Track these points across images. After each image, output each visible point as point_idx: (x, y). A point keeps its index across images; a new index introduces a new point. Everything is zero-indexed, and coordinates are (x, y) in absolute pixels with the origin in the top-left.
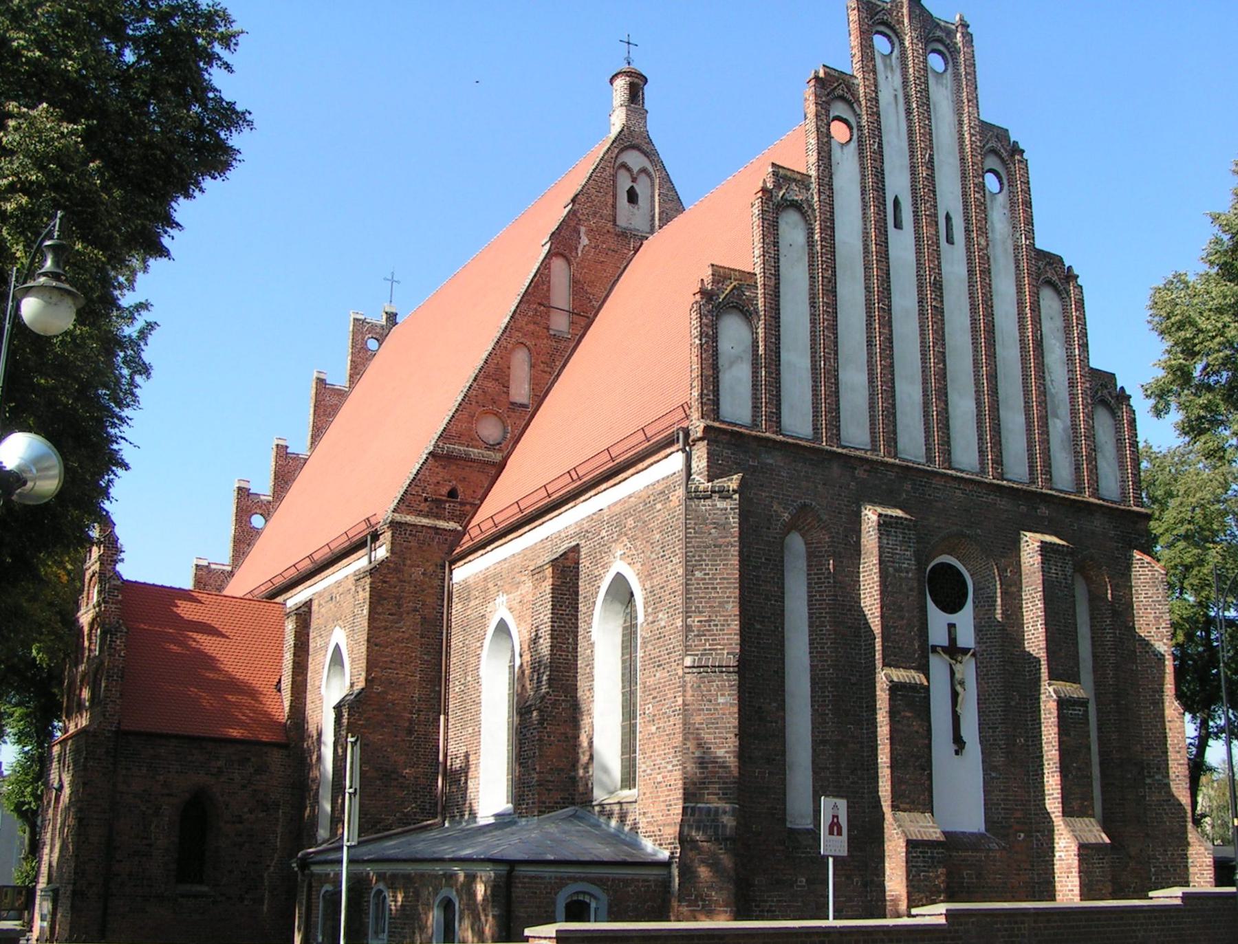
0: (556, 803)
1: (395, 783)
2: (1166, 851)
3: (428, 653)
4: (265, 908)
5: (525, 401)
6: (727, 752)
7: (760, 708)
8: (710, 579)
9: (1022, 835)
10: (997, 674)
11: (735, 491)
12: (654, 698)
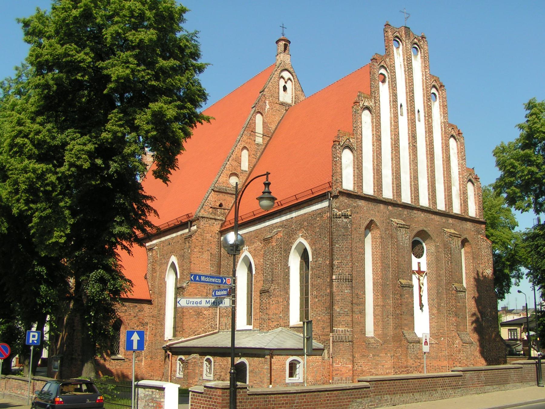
1: (201, 317)
2: (490, 344)
3: (213, 267)
4: (143, 364)
5: (247, 169)
7: (357, 293)
9: (443, 338)
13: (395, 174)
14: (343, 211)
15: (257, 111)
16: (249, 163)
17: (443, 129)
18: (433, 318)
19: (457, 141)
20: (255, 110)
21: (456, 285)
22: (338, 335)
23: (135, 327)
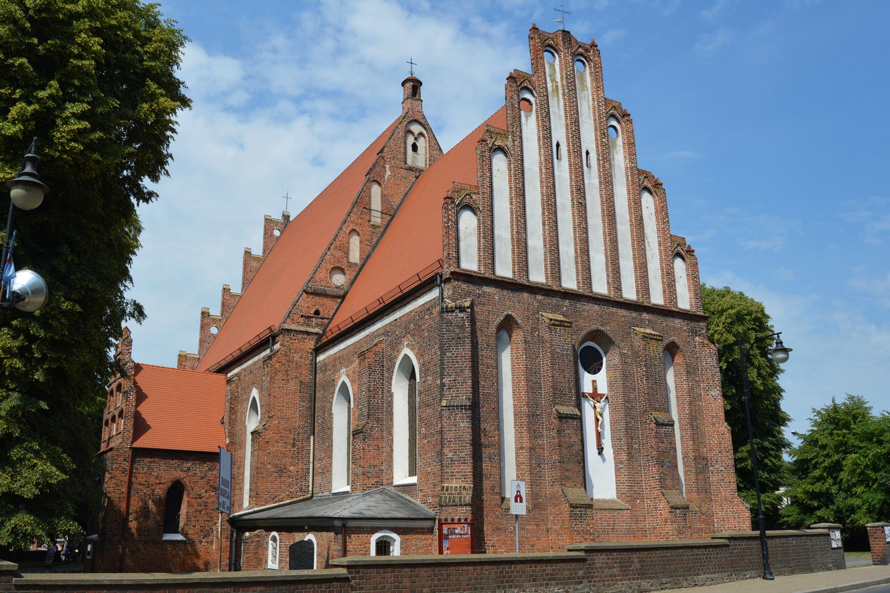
0: (372, 485)
3: (304, 402)
5: (358, 262)
6: (466, 455)
8: (455, 357)
9: (638, 501)
10: (621, 408)
11: (468, 308)
12: (425, 424)
13: (548, 246)
14: (458, 302)
15: (371, 179)
16: (360, 252)
17: (630, 178)
18: (620, 468)
19: (655, 195)
20: (369, 179)
21: (656, 414)
23: (203, 493)
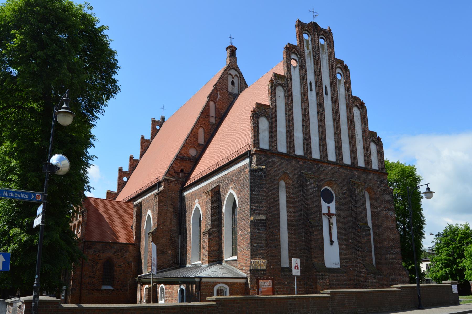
5: (203, 143)
9: (351, 269)
18: (342, 252)
22: (254, 265)
